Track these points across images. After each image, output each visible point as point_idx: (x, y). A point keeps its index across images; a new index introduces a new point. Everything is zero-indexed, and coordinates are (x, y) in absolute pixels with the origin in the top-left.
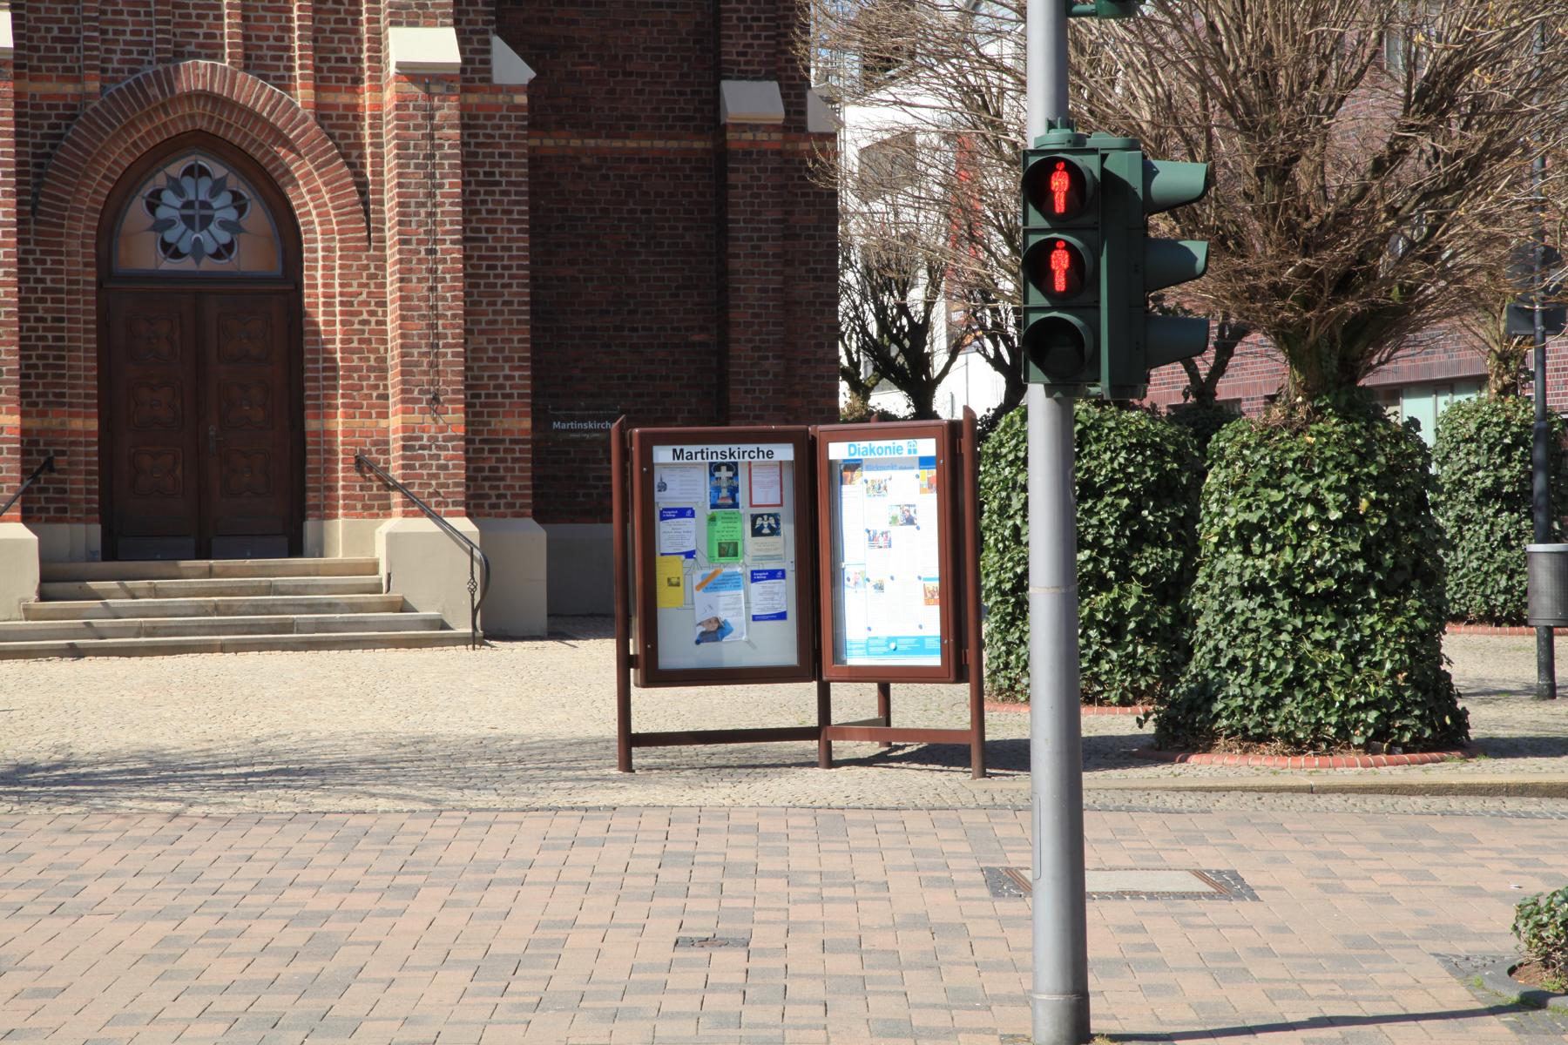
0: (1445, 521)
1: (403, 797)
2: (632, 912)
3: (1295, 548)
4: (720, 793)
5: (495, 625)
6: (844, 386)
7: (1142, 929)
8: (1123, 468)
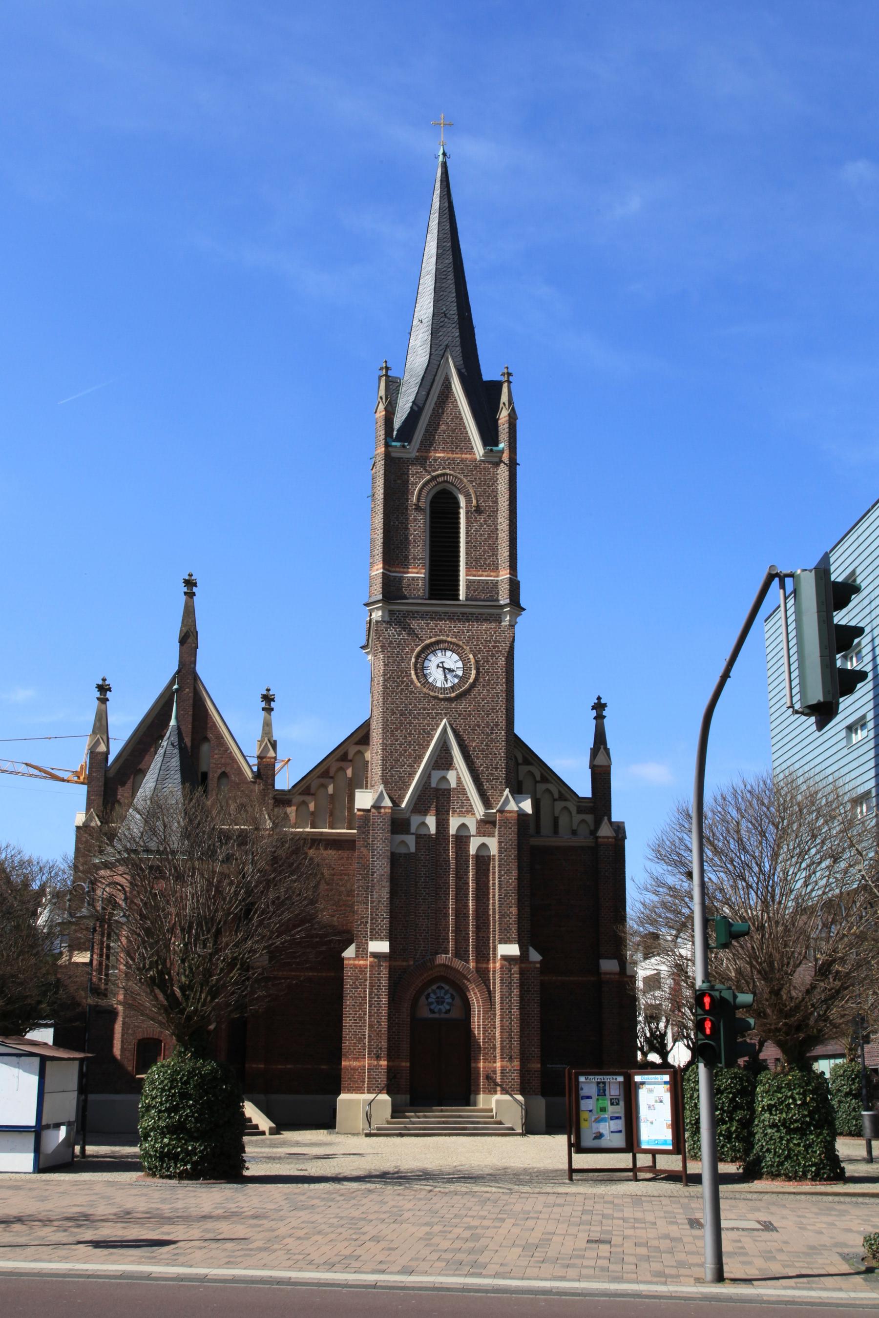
0: (834, 1103)
1: (500, 1187)
2: (573, 1230)
3: (786, 1113)
4: (601, 1189)
5: (530, 1129)
6: (639, 1053)
7: (740, 1241)
8: (730, 1084)
